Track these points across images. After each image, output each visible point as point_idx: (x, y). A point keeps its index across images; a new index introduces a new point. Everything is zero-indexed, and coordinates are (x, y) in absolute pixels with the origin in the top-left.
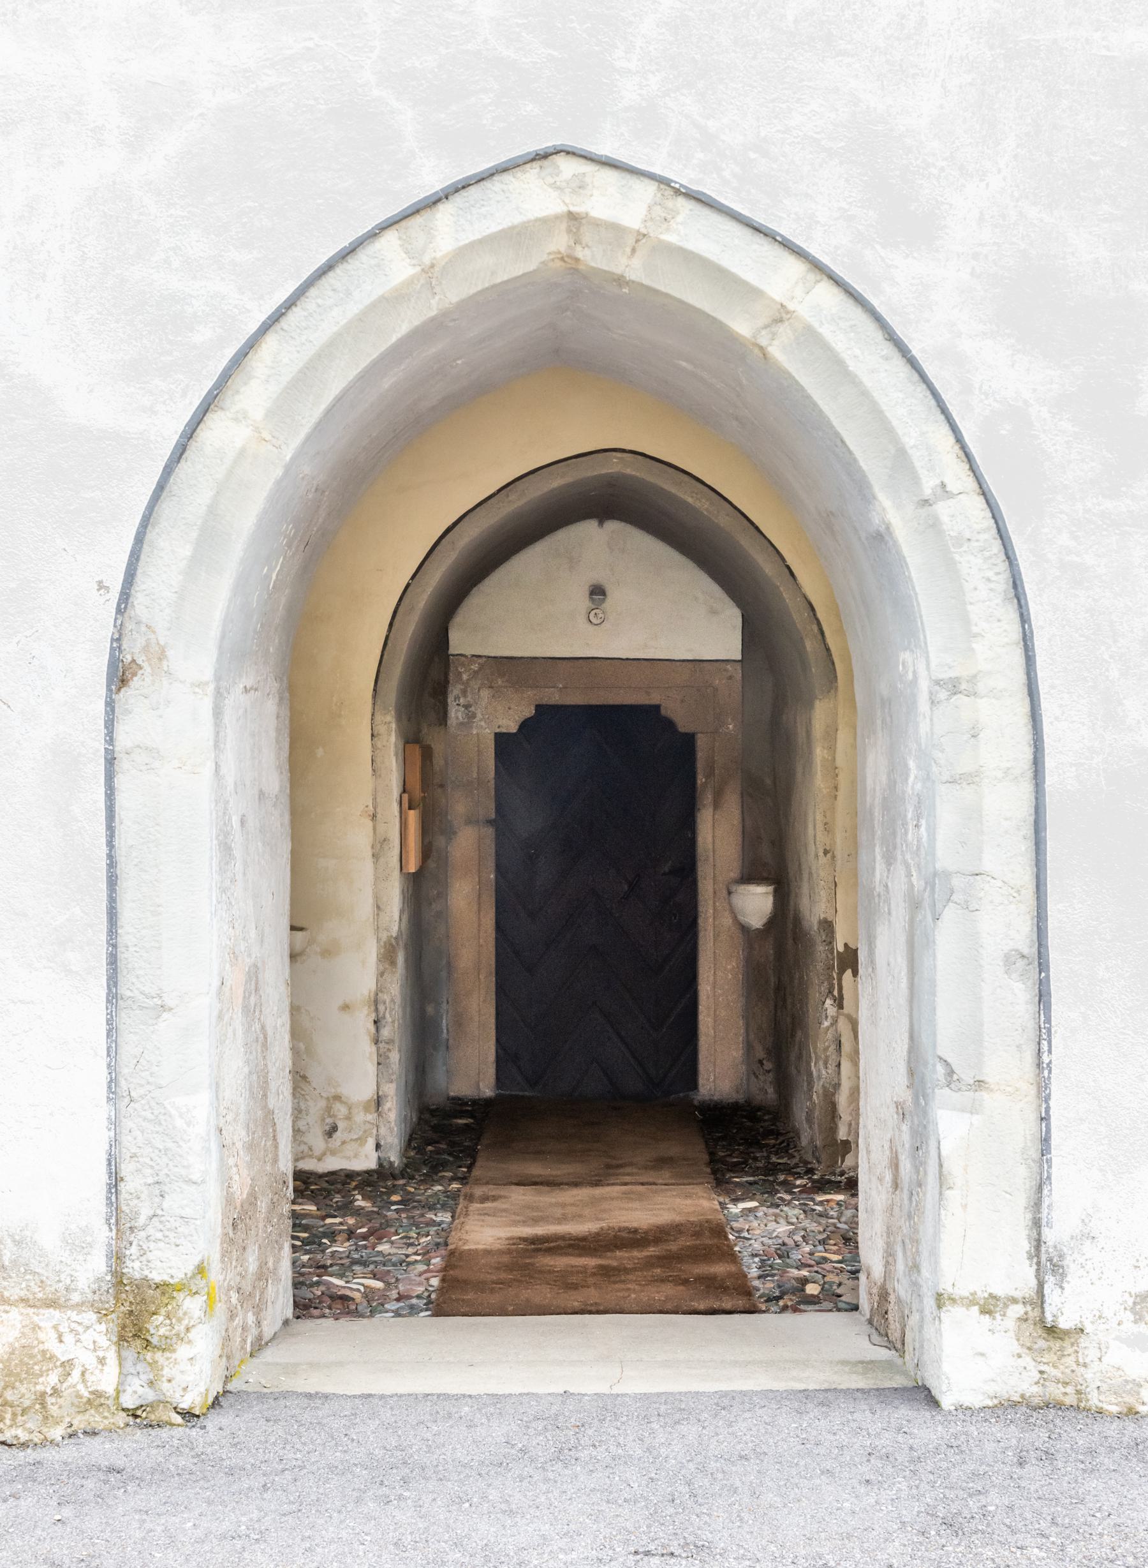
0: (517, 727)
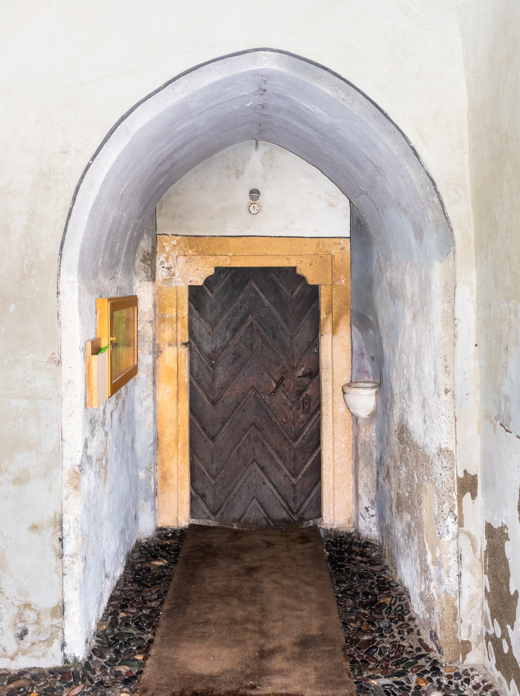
0: (203, 282)
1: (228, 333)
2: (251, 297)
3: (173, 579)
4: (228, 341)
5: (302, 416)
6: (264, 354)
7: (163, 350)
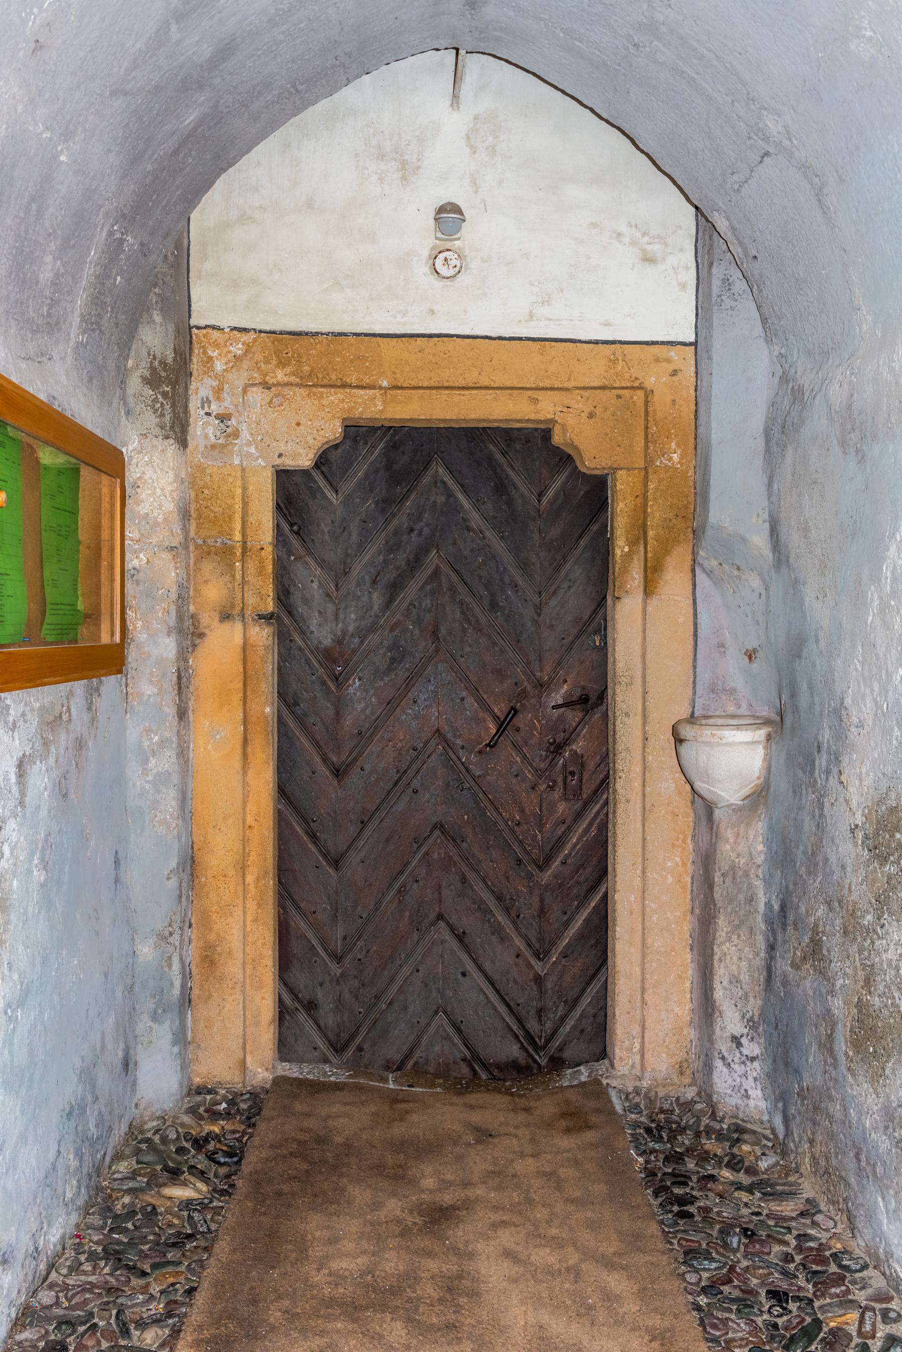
1: (375, 595)
2: (434, 504)
3: (217, 1249)
4: (377, 616)
5: (562, 807)
6: (468, 649)
7: (207, 631)
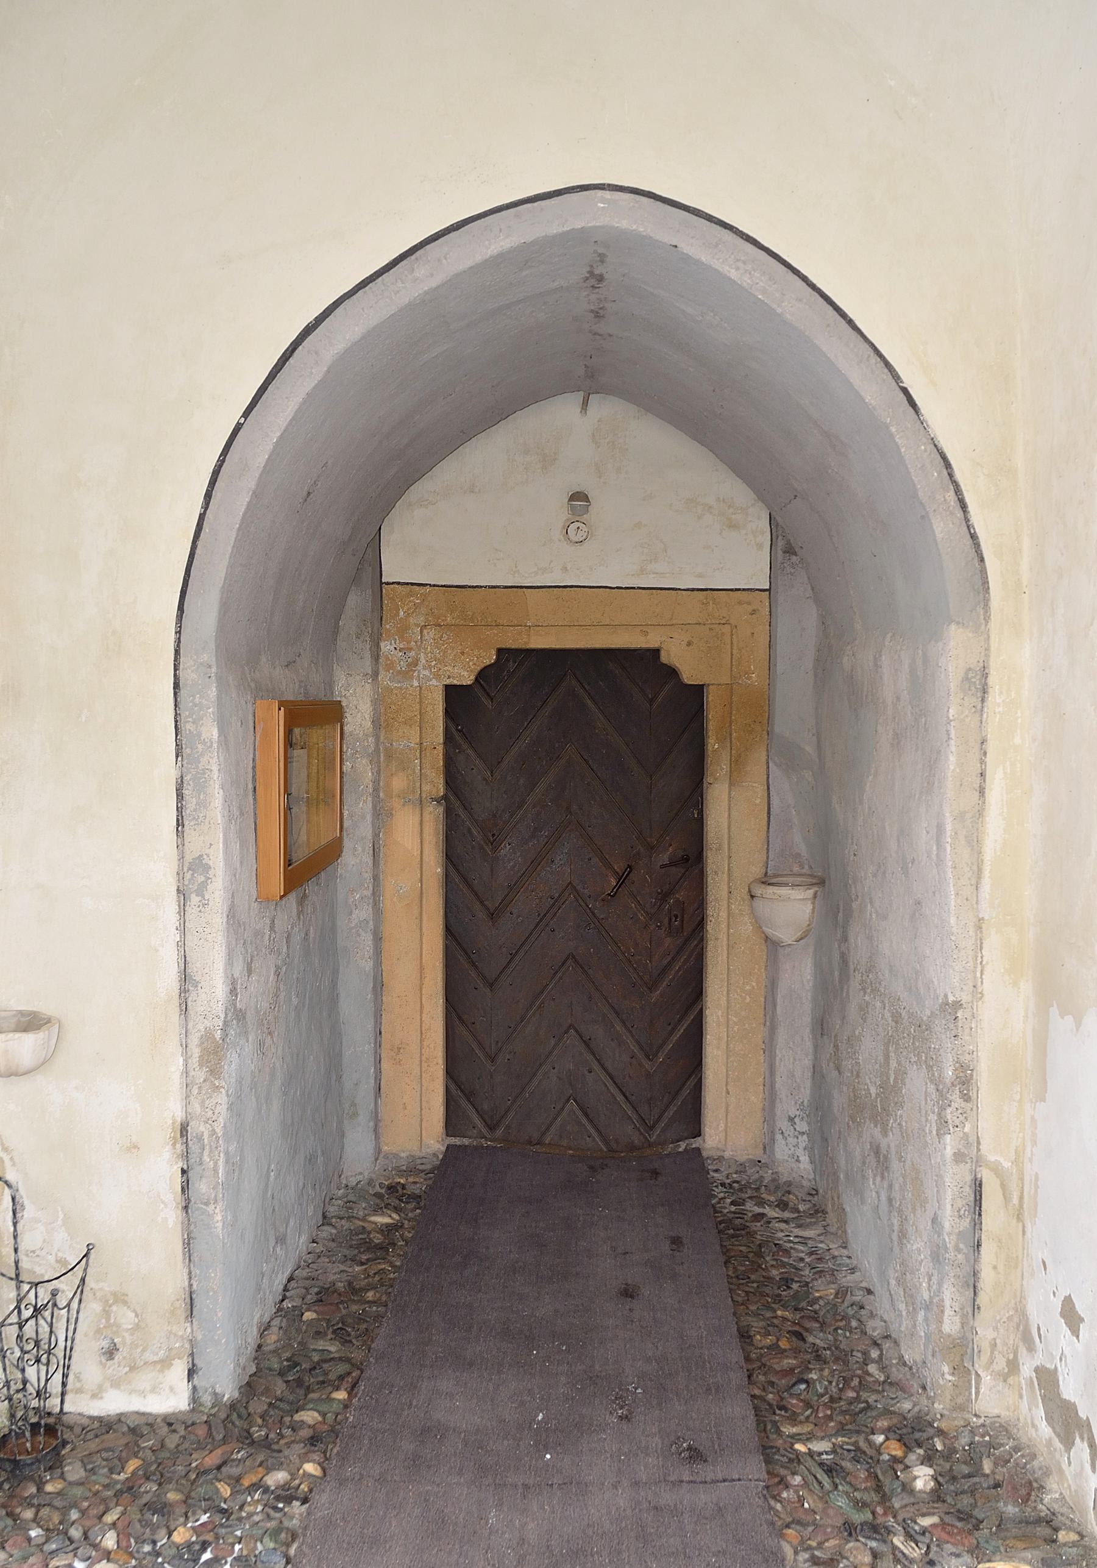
0: (473, 677)
